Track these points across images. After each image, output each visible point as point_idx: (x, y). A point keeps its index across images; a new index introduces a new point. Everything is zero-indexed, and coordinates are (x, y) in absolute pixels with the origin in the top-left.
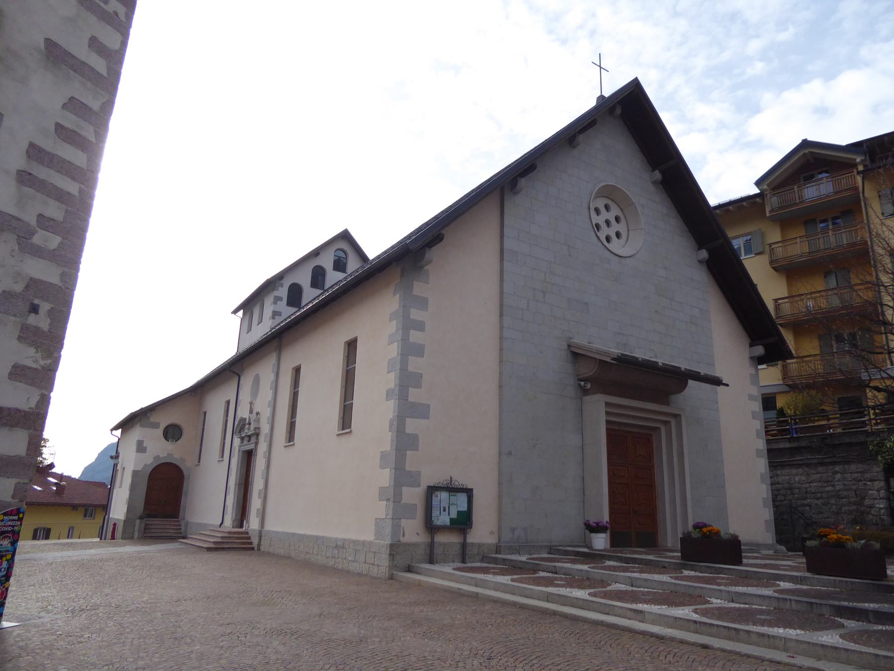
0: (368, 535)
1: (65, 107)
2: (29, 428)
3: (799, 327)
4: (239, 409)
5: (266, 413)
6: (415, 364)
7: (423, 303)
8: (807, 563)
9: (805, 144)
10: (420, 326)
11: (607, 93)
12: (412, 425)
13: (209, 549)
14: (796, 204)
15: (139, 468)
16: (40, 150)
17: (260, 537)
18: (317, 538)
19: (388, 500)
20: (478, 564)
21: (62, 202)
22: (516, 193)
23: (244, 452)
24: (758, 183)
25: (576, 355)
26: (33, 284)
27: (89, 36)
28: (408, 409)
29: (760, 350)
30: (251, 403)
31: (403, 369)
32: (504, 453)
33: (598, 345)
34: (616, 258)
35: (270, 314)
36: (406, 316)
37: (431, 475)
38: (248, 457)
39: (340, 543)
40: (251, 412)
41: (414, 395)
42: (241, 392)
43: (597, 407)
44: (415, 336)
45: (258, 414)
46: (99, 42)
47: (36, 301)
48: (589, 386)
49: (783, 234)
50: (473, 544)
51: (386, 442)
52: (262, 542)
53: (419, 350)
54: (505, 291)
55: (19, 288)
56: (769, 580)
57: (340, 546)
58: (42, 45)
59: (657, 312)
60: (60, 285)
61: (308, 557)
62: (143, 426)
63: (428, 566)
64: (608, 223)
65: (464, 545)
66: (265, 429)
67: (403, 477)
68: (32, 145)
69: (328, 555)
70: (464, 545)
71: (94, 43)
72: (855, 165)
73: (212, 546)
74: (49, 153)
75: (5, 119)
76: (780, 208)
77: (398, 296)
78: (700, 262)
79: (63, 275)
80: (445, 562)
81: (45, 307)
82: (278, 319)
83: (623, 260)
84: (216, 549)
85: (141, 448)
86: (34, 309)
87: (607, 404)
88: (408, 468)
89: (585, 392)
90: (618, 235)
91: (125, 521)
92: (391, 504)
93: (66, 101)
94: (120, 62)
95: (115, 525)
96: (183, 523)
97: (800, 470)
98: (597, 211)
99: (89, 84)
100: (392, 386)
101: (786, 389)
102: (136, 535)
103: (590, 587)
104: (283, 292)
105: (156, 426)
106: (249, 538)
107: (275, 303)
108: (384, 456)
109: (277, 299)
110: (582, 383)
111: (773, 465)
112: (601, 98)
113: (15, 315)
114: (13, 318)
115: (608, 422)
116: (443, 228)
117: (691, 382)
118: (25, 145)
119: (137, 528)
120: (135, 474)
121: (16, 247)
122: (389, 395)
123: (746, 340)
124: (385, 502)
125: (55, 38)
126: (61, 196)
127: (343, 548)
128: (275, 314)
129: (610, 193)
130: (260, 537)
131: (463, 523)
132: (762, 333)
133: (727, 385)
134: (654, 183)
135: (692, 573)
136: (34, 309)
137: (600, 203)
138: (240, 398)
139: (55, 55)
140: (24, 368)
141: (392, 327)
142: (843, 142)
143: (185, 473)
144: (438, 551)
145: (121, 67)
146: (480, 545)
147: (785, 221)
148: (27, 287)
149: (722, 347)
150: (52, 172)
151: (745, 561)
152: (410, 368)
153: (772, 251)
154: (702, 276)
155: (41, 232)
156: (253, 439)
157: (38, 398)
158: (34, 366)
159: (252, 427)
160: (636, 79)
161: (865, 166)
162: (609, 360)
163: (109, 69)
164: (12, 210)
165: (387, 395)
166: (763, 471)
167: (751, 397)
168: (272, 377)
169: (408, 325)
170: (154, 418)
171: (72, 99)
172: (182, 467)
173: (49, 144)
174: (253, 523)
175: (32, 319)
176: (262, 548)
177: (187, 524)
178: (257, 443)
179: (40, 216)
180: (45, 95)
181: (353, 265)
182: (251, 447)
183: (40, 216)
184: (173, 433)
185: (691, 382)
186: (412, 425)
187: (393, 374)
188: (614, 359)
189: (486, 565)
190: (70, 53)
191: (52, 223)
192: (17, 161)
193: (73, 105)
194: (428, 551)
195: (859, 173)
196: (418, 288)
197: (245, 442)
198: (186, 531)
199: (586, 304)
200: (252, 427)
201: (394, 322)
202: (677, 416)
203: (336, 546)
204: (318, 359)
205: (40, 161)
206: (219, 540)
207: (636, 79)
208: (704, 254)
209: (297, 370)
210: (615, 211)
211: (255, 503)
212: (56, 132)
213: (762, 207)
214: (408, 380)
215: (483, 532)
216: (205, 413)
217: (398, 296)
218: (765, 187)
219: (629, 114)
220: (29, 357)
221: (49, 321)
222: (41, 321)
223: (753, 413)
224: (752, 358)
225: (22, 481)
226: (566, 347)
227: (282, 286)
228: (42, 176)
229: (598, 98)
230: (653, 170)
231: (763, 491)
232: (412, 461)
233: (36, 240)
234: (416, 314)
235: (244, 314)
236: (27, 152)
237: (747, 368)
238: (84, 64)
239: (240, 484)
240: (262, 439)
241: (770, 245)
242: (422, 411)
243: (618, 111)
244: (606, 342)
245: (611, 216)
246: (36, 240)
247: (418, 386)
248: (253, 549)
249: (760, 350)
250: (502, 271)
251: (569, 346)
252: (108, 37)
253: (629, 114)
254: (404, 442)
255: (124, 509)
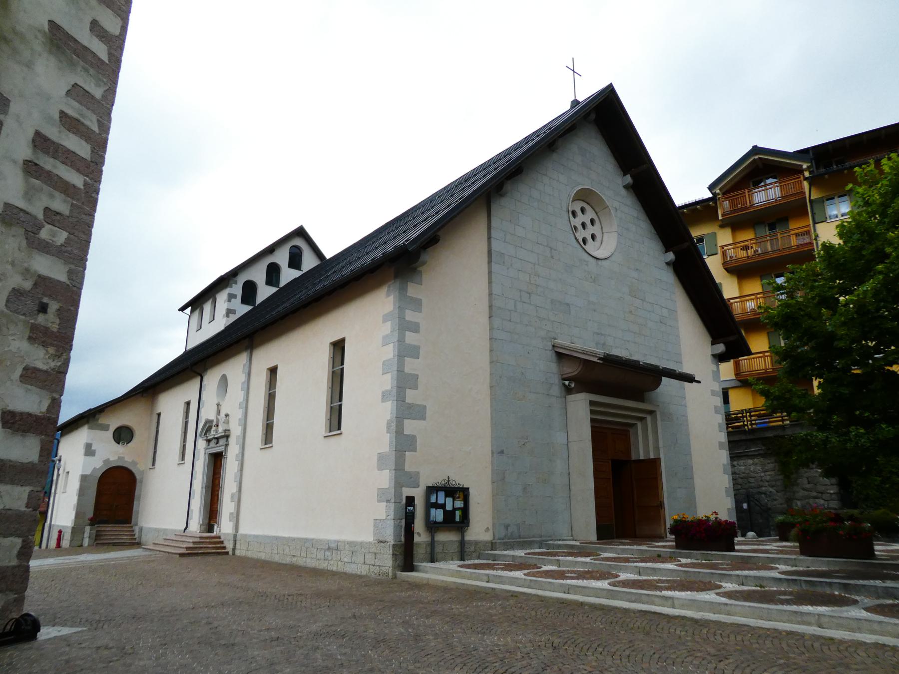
0: (368, 537)
1: (68, 93)
2: (41, 434)
3: (754, 324)
4: (202, 411)
5: (236, 415)
6: (411, 365)
7: (417, 304)
8: (801, 547)
9: (756, 150)
10: (415, 328)
11: (581, 98)
12: (410, 427)
13: (182, 555)
14: (746, 208)
15: (88, 472)
16: (46, 139)
17: (235, 541)
18: (305, 540)
19: (388, 501)
20: (477, 561)
21: (68, 195)
22: (502, 196)
23: (211, 455)
24: (711, 188)
25: (561, 356)
26: (42, 282)
27: (91, 19)
28: (406, 411)
29: (721, 348)
30: (218, 405)
31: (400, 371)
32: (499, 452)
33: (579, 345)
34: (593, 260)
35: (224, 312)
36: (401, 318)
37: (431, 476)
38: (216, 460)
39: (332, 545)
40: (219, 412)
41: (411, 396)
42: (204, 393)
43: (580, 406)
44: (411, 338)
45: (227, 415)
46: (100, 26)
47: (45, 300)
48: (573, 386)
49: (734, 237)
50: (470, 542)
51: (385, 443)
52: (238, 546)
53: (413, 352)
54: (494, 292)
55: (28, 285)
56: (766, 565)
57: (334, 548)
58: (46, 27)
59: (631, 312)
60: (68, 282)
61: (294, 559)
62: (90, 428)
63: (430, 564)
64: (584, 225)
65: (462, 543)
66: (236, 431)
67: (402, 477)
68: (37, 133)
69: (319, 557)
70: (462, 543)
71: (95, 27)
72: (801, 171)
73: (184, 551)
74: (54, 143)
75: (11, 104)
76: (732, 212)
77: (391, 298)
78: (668, 264)
79: (70, 273)
80: (444, 559)
81: (53, 306)
82: (233, 318)
83: (600, 262)
84: (189, 555)
85: (89, 451)
86: (43, 309)
87: (592, 403)
88: (407, 469)
89: (568, 391)
90: (593, 237)
91: (73, 528)
92: (392, 505)
93: (69, 87)
94: (121, 48)
95: (60, 532)
96: (137, 529)
97: (756, 460)
98: (574, 214)
99: (92, 71)
100: (389, 387)
101: (738, 384)
102: (86, 542)
103: (607, 578)
104: (237, 289)
105: (105, 428)
106: (222, 542)
107: (229, 301)
108: (381, 457)
109: (231, 297)
110: (567, 383)
111: (734, 457)
112: (575, 103)
113: (24, 314)
114: (23, 317)
115: (592, 420)
116: (439, 229)
117: (665, 380)
118: (31, 134)
119: (86, 535)
120: (84, 478)
121: (24, 243)
122: (385, 396)
123: (708, 339)
124: (385, 503)
125: (58, 21)
126: (66, 188)
127: (337, 549)
128: (229, 312)
129: (586, 197)
130: (235, 541)
131: (457, 521)
132: (725, 330)
133: (699, 382)
134: (626, 187)
135: (689, 561)
136: (43, 309)
137: (577, 207)
138: (203, 398)
139: (58, 39)
140: (36, 370)
141: (387, 328)
142: (791, 149)
143: (138, 477)
144: (438, 549)
145: (121, 55)
146: (476, 543)
147: (735, 224)
148: (36, 285)
149: (687, 344)
150: (58, 164)
151: (737, 547)
152: (407, 370)
153: (724, 254)
154: (669, 277)
155: (48, 227)
156: (222, 442)
157: (49, 401)
158: (45, 367)
159: (221, 429)
160: (611, 85)
161: (810, 173)
162: (595, 360)
163: (110, 54)
164: (21, 203)
165: (383, 396)
166: (725, 462)
167: (713, 393)
168: (243, 378)
169: (405, 327)
170: (103, 420)
171: (75, 85)
172: (134, 470)
173: (54, 133)
174: (225, 527)
175: (41, 319)
176: (238, 553)
177: (141, 529)
178: (227, 445)
179: (47, 210)
180: (46, 83)
181: (309, 262)
182: (222, 449)
183: (47, 210)
184: (123, 435)
185: (665, 380)
186: (410, 427)
187: (389, 376)
188: (600, 359)
189: (485, 562)
190: (72, 37)
191: (58, 217)
192: (24, 151)
193: (76, 92)
194: (429, 549)
195: (805, 179)
196: (412, 290)
197: (212, 444)
198: (140, 537)
199: (568, 305)
200: (221, 429)
201: (389, 323)
202: (651, 413)
203: (329, 549)
204: (299, 357)
205: (46, 152)
206: (191, 545)
207: (611, 85)
208: (671, 256)
209: (273, 371)
210: (590, 214)
211: (227, 507)
212: (61, 121)
213: (715, 209)
214: (405, 382)
215: (480, 528)
216: (159, 415)
217: (391, 298)
218: (718, 191)
219: (604, 118)
220: (40, 358)
221: (58, 321)
222: (50, 320)
223: (716, 407)
224: (714, 356)
225: (36, 489)
226: (551, 348)
227: (236, 283)
228: (48, 167)
229: (573, 102)
230: (625, 175)
231: (725, 481)
232: (411, 463)
233: (44, 234)
234: (410, 316)
235: (192, 312)
236: (33, 141)
237: (710, 365)
238: (86, 48)
239: (207, 487)
240: (232, 440)
241: (722, 247)
242: (419, 412)
243: (593, 116)
244: (588, 342)
245: (586, 218)
246: (44, 234)
247: (415, 387)
248: (227, 553)
249: (721, 348)
250: (490, 273)
251: (554, 346)
252: (110, 24)
253: (604, 118)
254: (404, 444)
255: (72, 515)
